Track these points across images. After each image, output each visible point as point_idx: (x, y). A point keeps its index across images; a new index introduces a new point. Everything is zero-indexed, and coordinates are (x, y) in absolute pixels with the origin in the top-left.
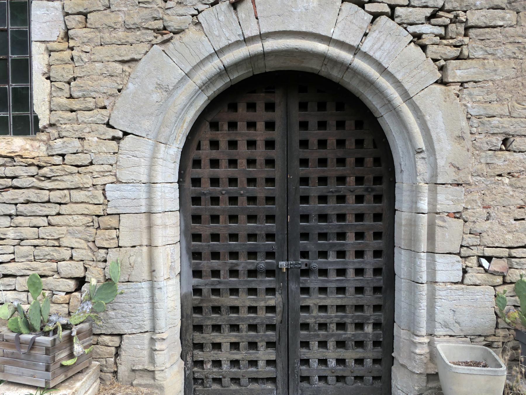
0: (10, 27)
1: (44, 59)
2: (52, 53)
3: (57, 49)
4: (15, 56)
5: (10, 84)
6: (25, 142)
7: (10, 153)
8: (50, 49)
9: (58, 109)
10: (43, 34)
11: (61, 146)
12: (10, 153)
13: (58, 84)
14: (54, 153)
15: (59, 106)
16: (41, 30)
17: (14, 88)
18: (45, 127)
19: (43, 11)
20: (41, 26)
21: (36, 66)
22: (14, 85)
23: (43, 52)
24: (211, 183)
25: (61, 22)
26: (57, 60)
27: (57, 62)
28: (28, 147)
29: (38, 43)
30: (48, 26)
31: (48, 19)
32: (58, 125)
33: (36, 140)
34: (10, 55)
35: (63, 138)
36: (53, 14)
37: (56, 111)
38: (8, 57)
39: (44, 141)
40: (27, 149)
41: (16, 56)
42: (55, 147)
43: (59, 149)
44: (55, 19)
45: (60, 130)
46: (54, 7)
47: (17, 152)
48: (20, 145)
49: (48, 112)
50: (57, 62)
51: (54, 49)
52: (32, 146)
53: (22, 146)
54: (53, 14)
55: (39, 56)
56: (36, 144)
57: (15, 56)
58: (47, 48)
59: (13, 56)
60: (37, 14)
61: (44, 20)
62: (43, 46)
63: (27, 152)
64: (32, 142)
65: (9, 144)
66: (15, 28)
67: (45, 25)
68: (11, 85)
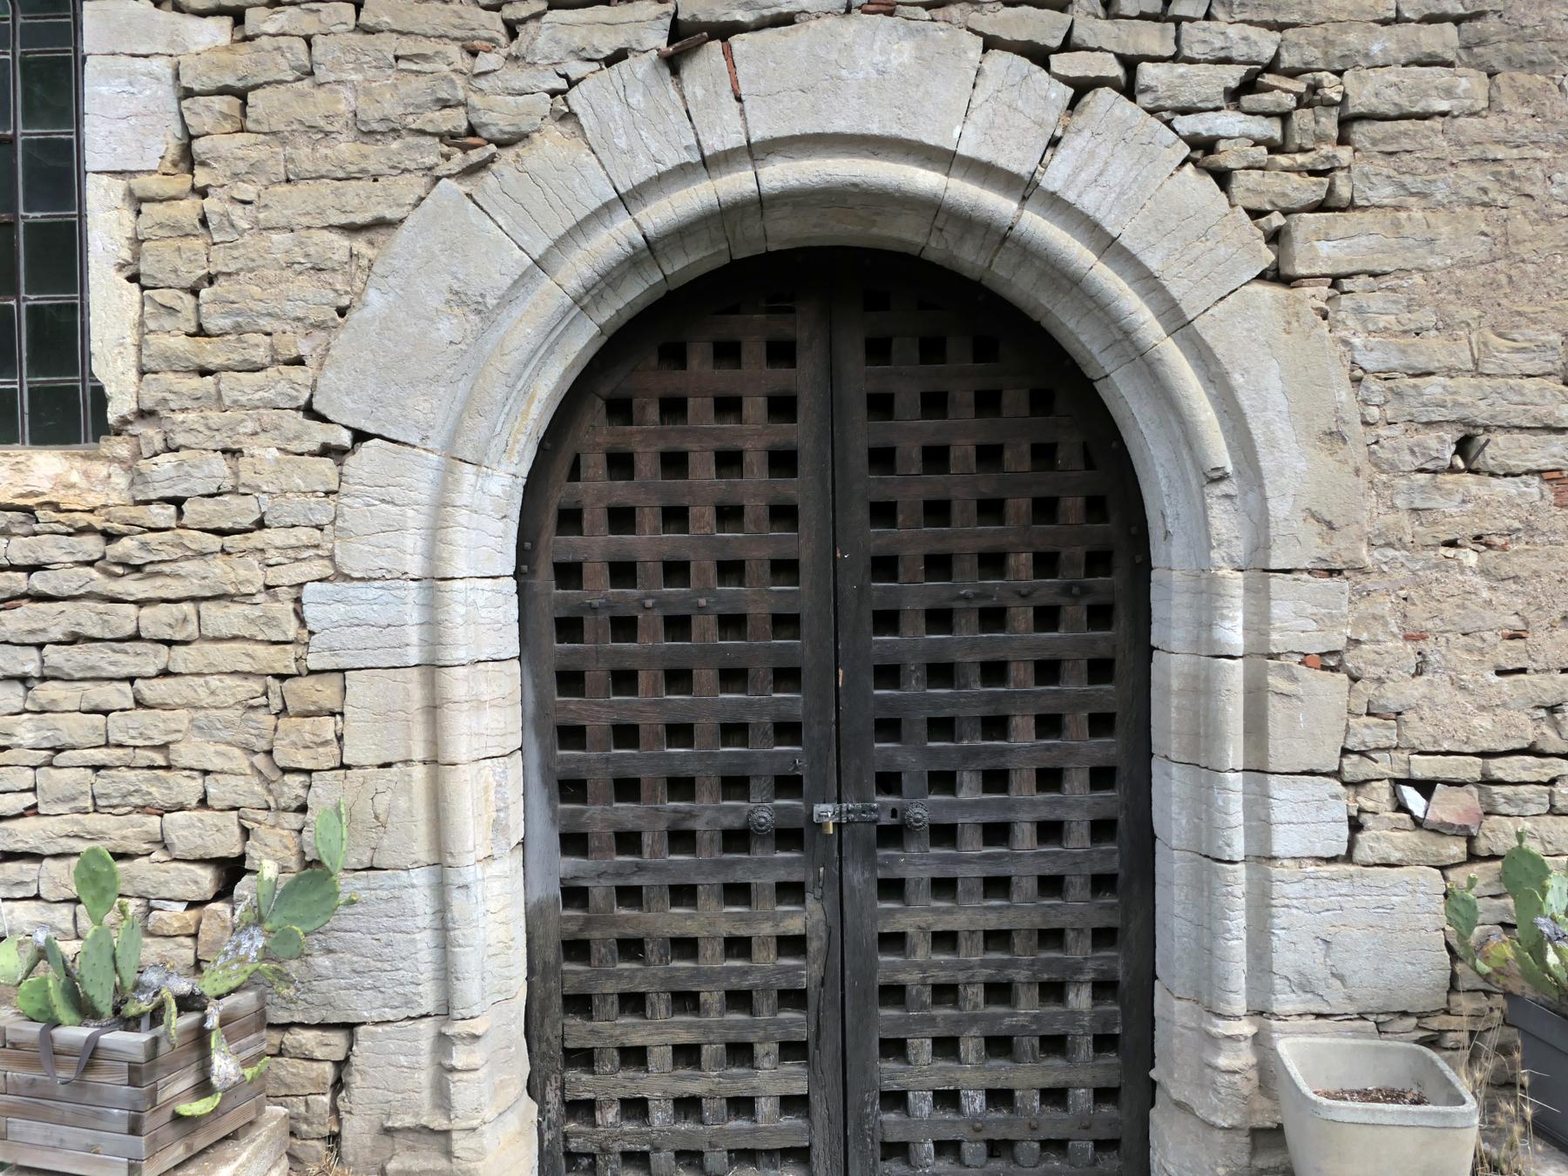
0: (20, 130)
1: (120, 224)
5: (23, 294)
6: (67, 464)
7: (22, 496)
8: (138, 193)
10: (119, 150)
11: (174, 474)
14: (153, 496)
15: (167, 359)
16: (112, 139)
17: (34, 306)
23: (120, 204)
26: (161, 225)
27: (160, 233)
28: (75, 477)
30: (133, 128)
32: (164, 413)
33: (98, 458)
34: (22, 212)
35: (177, 450)
36: (148, 92)
39: (121, 461)
40: (73, 486)
41: (39, 214)
42: (155, 477)
43: (165, 484)
44: (152, 107)
45: (168, 427)
47: (43, 494)
50: (160, 233)
52: (86, 475)
53: (57, 475)
54: (148, 92)
56: (100, 469)
58: (130, 193)
60: (100, 95)
61: (121, 112)
62: (119, 185)
63: (71, 492)
64: (87, 464)
66: (37, 133)
67: (123, 124)
68: (25, 299)
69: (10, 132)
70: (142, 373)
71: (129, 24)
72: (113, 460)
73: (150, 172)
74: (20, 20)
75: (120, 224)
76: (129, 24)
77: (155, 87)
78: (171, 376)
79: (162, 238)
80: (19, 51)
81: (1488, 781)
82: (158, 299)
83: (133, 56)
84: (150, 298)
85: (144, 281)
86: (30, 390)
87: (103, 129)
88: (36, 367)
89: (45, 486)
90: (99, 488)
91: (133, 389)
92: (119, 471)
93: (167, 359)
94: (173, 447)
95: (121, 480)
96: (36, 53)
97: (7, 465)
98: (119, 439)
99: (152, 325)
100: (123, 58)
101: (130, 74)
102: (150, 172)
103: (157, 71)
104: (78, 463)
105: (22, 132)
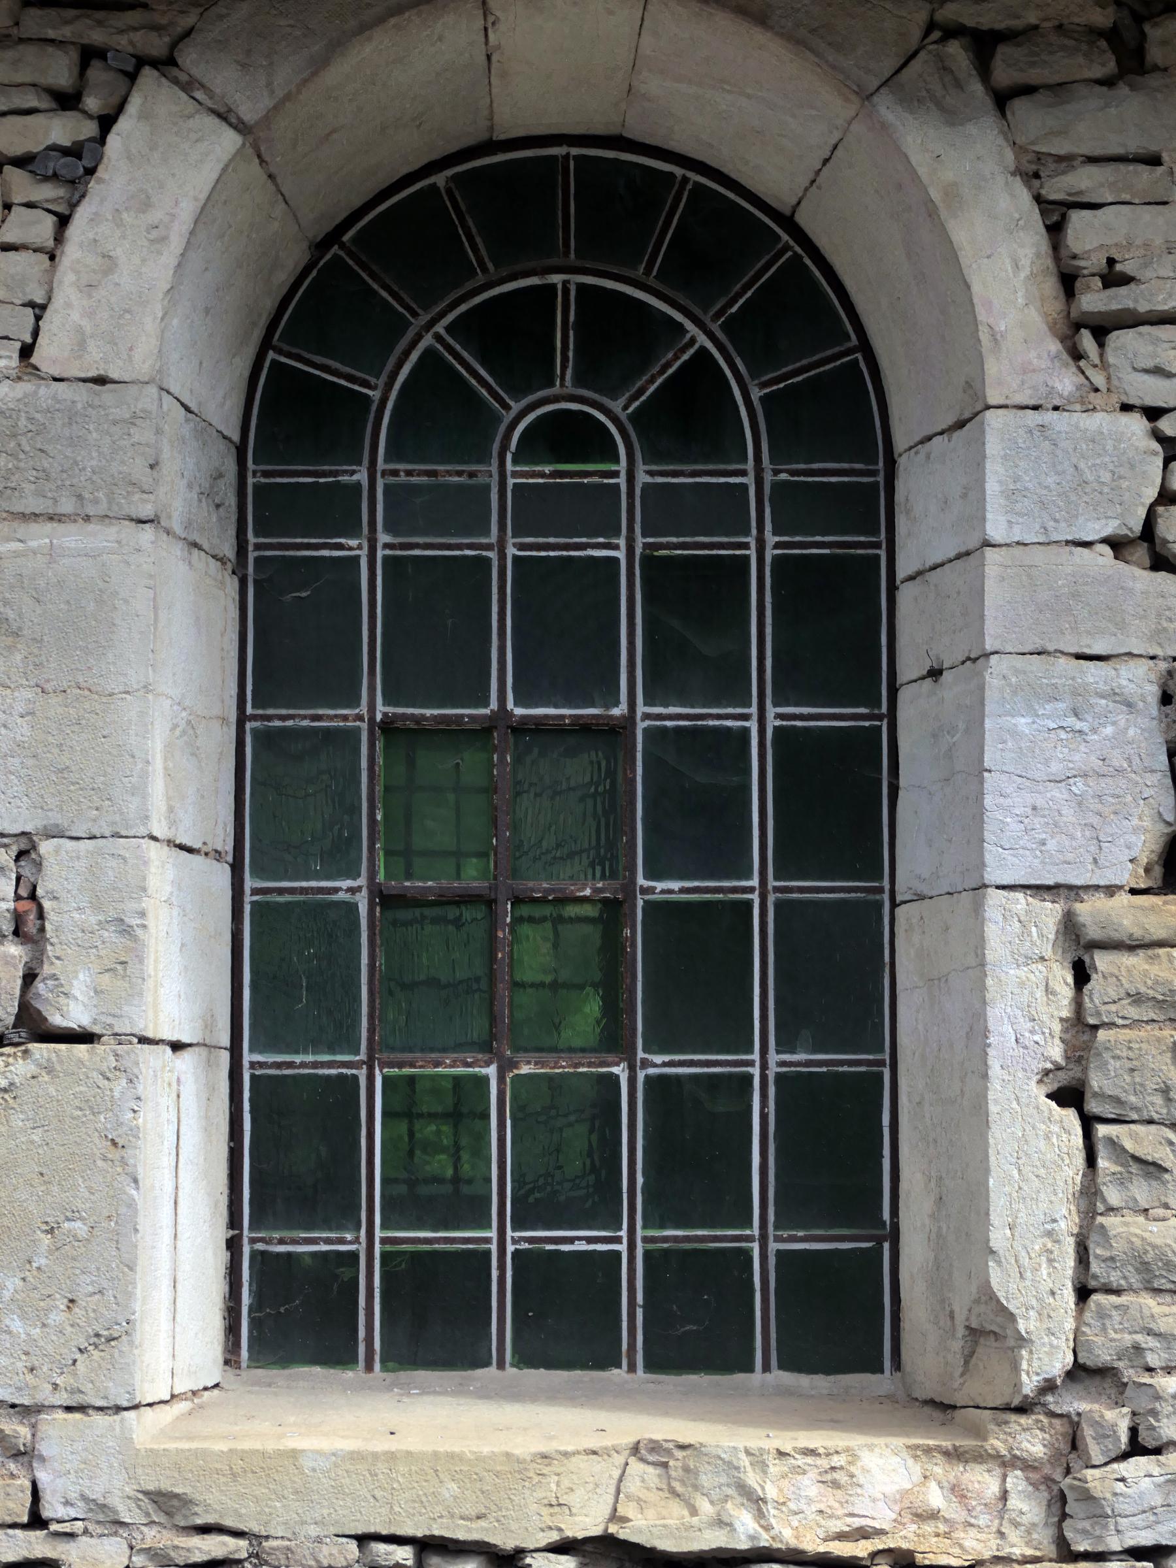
0: (641, 709)
1: (1048, 991)
2: (1102, 961)
3: (1138, 933)
4: (670, 887)
5: (641, 1054)
6: (916, 1469)
7: (841, 1536)
8: (1093, 932)
9: (1134, 1280)
10: (1052, 845)
11: (1158, 1500)
12: (841, 1536)
13: (1133, 1136)
14: (1115, 1544)
15: (1144, 1267)
16: (1037, 822)
17: (662, 1077)
18: (1049, 1387)
19: (1053, 713)
20: (1040, 802)
21: (1008, 1029)
22: (659, 1063)
23: (1048, 953)
24: (873, 1372)
25: (1151, 779)
26: (1137, 999)
27: (1133, 1012)
28: (936, 1498)
29: (1019, 895)
30: (1080, 802)
31: (1081, 757)
32: (1129, 1374)
33: (980, 1457)
34: (641, 881)
35: (1157, 1451)
36: (1109, 730)
37: (1117, 1292)
38: (629, 887)
39: (1027, 1465)
40: (934, 1515)
41: (675, 885)
42: (1122, 1506)
43: (1138, 1520)
44: (1118, 761)
45: (1144, 1404)
46: (1114, 695)
47: (881, 1532)
48: (891, 1489)
49: (1069, 1296)
50: (1133, 1012)
51: (1116, 936)
52: (957, 1491)
53: (905, 1493)
54: (1109, 730)
55: (1023, 972)
56: (983, 1481)
57: (670, 887)
58: (1070, 927)
59: (660, 886)
60: (1014, 733)
61: (1056, 768)
62: (1050, 912)
63: (929, 1528)
64: (957, 1472)
65: (836, 1485)
66: (675, 714)
67: (1058, 793)
68: (645, 1064)
69: (616, 712)
70: (1083, 1293)
71: (1075, 595)
72: (1008, 1463)
73: (1111, 890)
74: (642, 478)
75: (1048, 991)
76: (1075, 595)
77: (1122, 719)
78: (1149, 1302)
79: (1136, 1023)
80: (640, 541)
81: (559, 920)
82: (1129, 1145)
83: (1079, 657)
84: (1112, 1142)
85: (1093, 1107)
86: (647, 1255)
87: (1020, 802)
88: (661, 1208)
89: (883, 1517)
90: (983, 1520)
91: (1070, 1324)
92: (1023, 1485)
93: (1144, 1267)
94: (1151, 1444)
95: (1027, 1505)
96: (675, 545)
97: (813, 1474)
98: (1024, 1420)
99: (1113, 1196)
100: (1062, 660)
101: (1075, 693)
102: (1111, 890)
103: (1130, 689)
104: (939, 1468)
105: (647, 714)
